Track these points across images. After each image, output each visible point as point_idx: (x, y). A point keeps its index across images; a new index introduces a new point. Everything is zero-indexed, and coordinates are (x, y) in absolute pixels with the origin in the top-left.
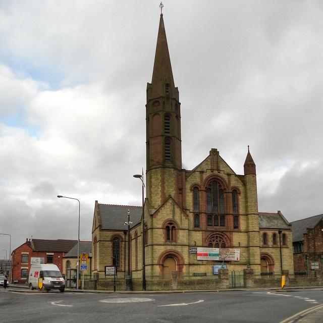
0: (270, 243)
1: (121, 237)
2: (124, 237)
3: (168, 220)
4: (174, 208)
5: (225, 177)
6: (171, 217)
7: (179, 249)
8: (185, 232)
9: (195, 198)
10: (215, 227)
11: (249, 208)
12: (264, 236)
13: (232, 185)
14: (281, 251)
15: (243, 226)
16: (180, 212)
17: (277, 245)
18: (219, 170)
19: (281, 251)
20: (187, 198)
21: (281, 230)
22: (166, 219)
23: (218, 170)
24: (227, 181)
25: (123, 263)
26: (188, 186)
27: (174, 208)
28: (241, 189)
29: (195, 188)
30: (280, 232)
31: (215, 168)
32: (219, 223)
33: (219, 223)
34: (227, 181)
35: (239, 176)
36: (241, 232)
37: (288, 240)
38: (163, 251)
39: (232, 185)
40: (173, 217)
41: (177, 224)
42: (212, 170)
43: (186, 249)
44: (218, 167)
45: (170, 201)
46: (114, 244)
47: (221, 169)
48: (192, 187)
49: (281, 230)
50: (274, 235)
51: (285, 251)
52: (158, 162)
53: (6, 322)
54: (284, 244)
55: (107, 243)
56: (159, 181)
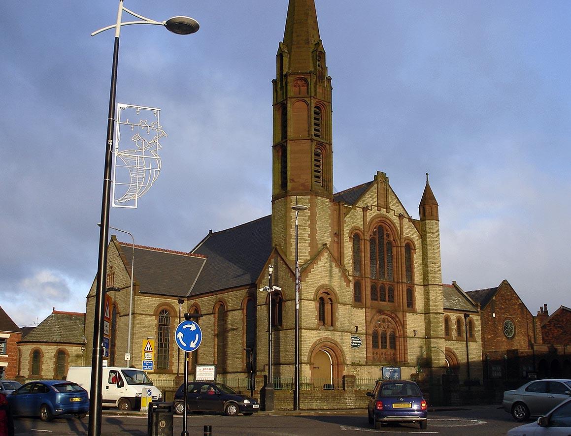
0: (454, 334)
1: (173, 308)
2: (178, 309)
3: (322, 287)
4: (331, 266)
5: (396, 220)
6: (326, 281)
7: (337, 337)
8: (346, 309)
9: (357, 252)
10: (380, 302)
11: (430, 275)
12: (458, 323)
13: (405, 235)
14: (467, 346)
15: (419, 304)
16: (340, 274)
17: (463, 337)
18: (388, 209)
19: (467, 346)
20: (346, 251)
21: (467, 313)
22: (320, 284)
23: (387, 209)
24: (398, 226)
25: (176, 357)
26: (346, 231)
27: (331, 266)
28: (418, 242)
29: (356, 238)
30: (466, 316)
31: (382, 203)
32: (387, 297)
33: (387, 297)
34: (398, 226)
35: (414, 222)
36: (417, 313)
37: (284, 324)
38: (315, 340)
39: (405, 235)
40: (330, 281)
41: (336, 295)
42: (379, 207)
43: (348, 338)
44: (387, 203)
45: (326, 255)
46: (160, 321)
47: (392, 207)
48: (351, 232)
49: (467, 313)
50: (459, 321)
51: (472, 345)
52: (303, 185)
53: (329, 435)
54: (472, 335)
55: (149, 318)
56: (307, 219)
